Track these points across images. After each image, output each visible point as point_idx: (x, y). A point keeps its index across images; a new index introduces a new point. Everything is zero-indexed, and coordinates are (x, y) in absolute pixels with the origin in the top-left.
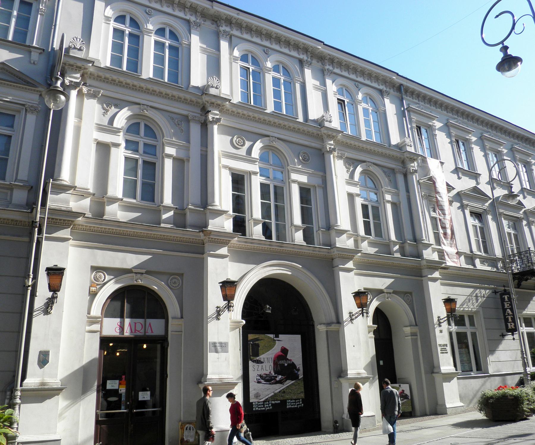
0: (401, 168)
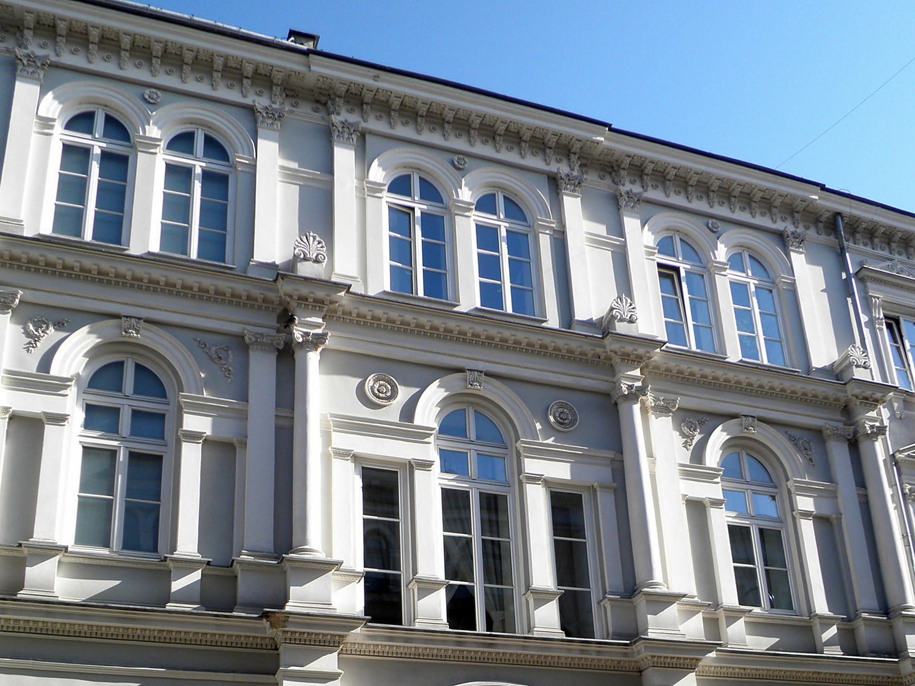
0: (840, 425)
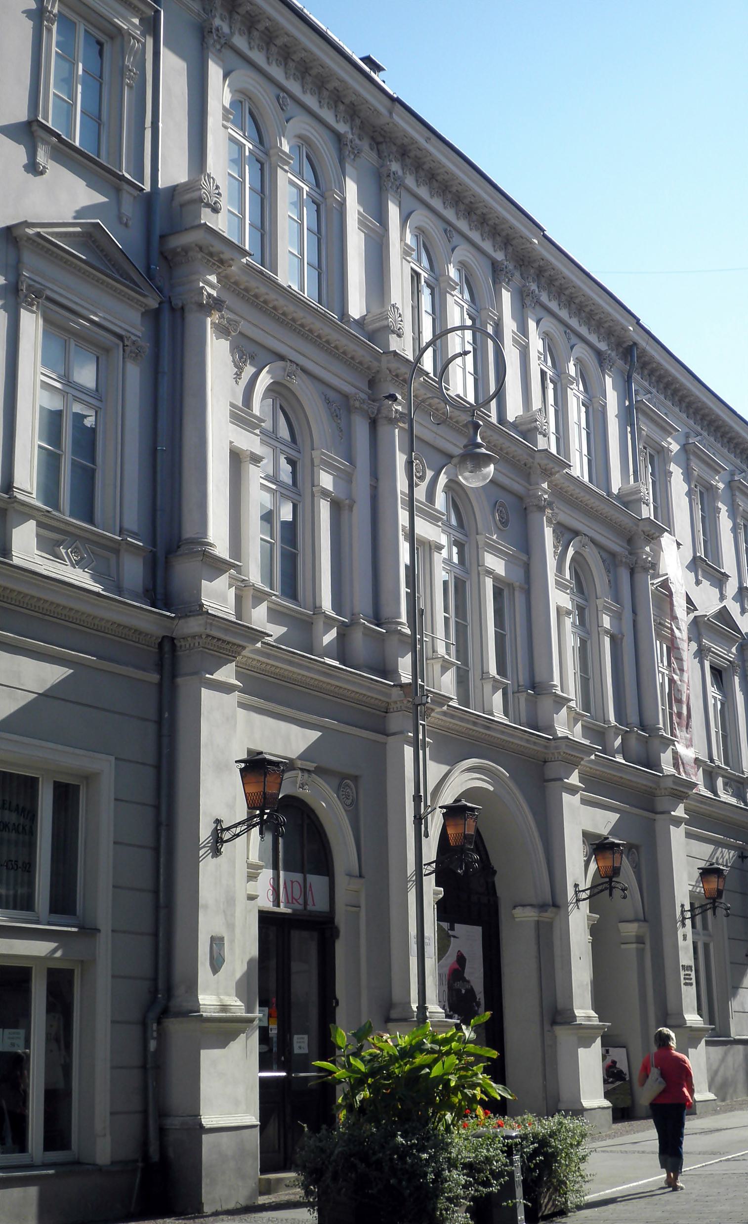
0: (363, 396)
